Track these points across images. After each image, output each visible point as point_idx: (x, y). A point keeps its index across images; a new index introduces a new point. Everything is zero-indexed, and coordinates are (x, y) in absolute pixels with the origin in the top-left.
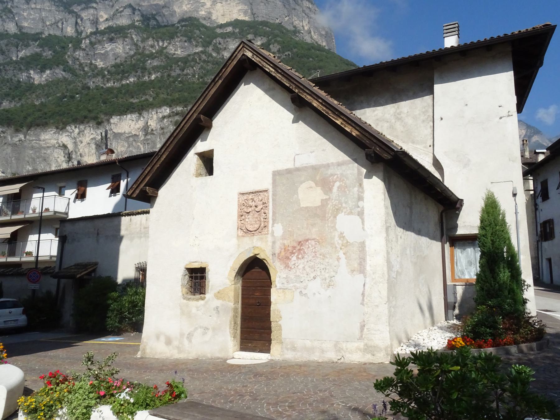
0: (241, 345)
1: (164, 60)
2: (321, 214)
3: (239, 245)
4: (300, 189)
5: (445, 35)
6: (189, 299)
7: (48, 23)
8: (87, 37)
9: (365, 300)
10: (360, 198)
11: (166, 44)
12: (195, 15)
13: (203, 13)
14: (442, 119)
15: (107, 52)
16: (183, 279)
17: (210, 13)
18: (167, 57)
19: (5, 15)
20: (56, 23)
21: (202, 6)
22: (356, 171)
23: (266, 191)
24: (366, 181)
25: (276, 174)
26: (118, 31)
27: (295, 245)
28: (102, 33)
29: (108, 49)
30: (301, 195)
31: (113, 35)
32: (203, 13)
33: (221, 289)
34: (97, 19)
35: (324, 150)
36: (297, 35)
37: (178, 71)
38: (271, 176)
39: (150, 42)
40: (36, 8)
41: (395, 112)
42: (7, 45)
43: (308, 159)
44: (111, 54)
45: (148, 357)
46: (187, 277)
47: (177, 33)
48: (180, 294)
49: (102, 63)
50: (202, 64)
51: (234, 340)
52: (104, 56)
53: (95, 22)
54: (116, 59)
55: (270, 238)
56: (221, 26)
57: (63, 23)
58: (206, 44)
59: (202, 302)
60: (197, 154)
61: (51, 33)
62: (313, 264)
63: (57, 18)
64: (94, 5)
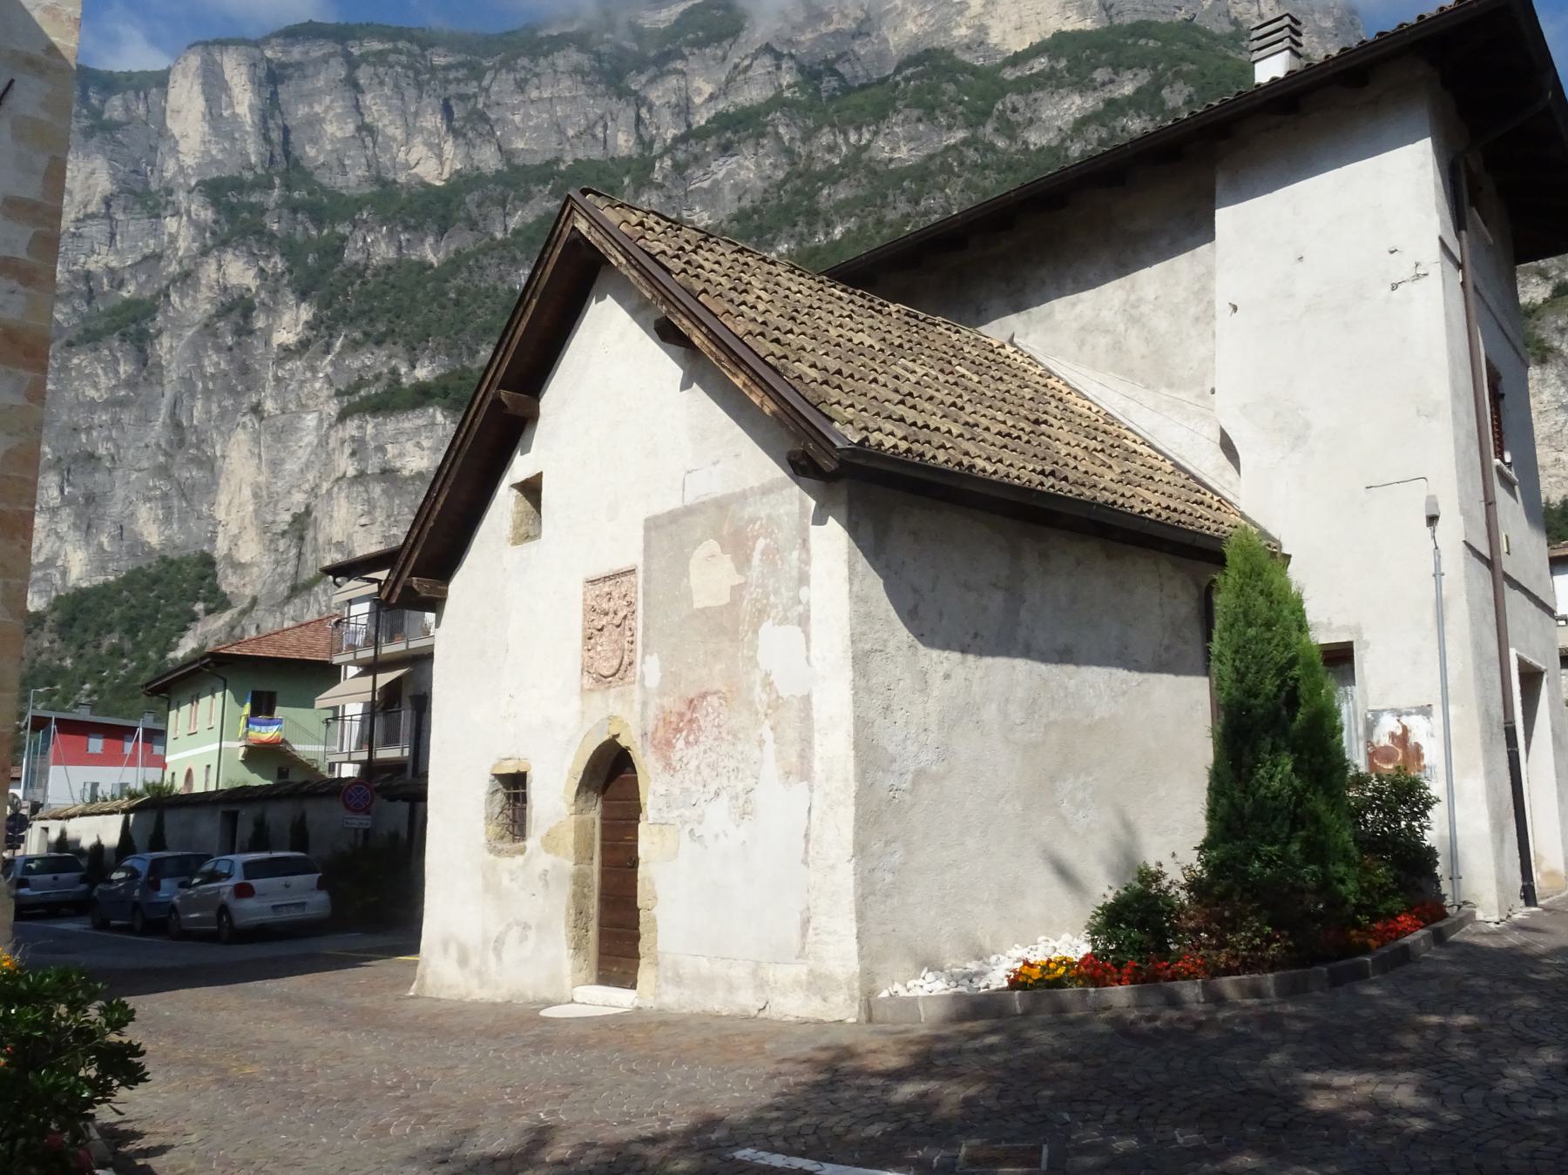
0: (599, 969)
1: (864, 181)
2: (730, 625)
3: (583, 713)
4: (692, 561)
5: (1256, 55)
6: (499, 853)
7: (571, 133)
8: (668, 150)
9: (812, 853)
10: (803, 579)
11: (867, 136)
12: (940, 42)
13: (963, 31)
14: (1235, 308)
15: (716, 183)
16: (490, 802)
17: (983, 29)
18: (873, 173)
19: (473, 129)
20: (591, 127)
21: (960, 13)
22: (796, 507)
23: (632, 571)
24: (814, 530)
25: (653, 526)
26: (740, 122)
27: (683, 708)
28: (702, 134)
29: (720, 175)
30: (694, 579)
31: (729, 134)
32: (962, 32)
33: (553, 824)
34: (688, 99)
35: (737, 456)
36: (1244, 44)
37: (904, 207)
38: (641, 532)
39: (825, 138)
40: (541, 99)
41: (1126, 302)
42: (479, 206)
43: (710, 485)
44: (727, 186)
45: (428, 994)
46: (500, 796)
47: (895, 99)
48: (483, 840)
49: (705, 215)
50: (967, 175)
51: (575, 956)
52: (711, 196)
53: (684, 109)
54: (740, 199)
55: (637, 695)
56: (1017, 59)
57: (605, 127)
58: (977, 117)
59: (519, 859)
60: (514, 486)
61: (580, 156)
62: (714, 756)
63: (592, 116)
64: (679, 65)
